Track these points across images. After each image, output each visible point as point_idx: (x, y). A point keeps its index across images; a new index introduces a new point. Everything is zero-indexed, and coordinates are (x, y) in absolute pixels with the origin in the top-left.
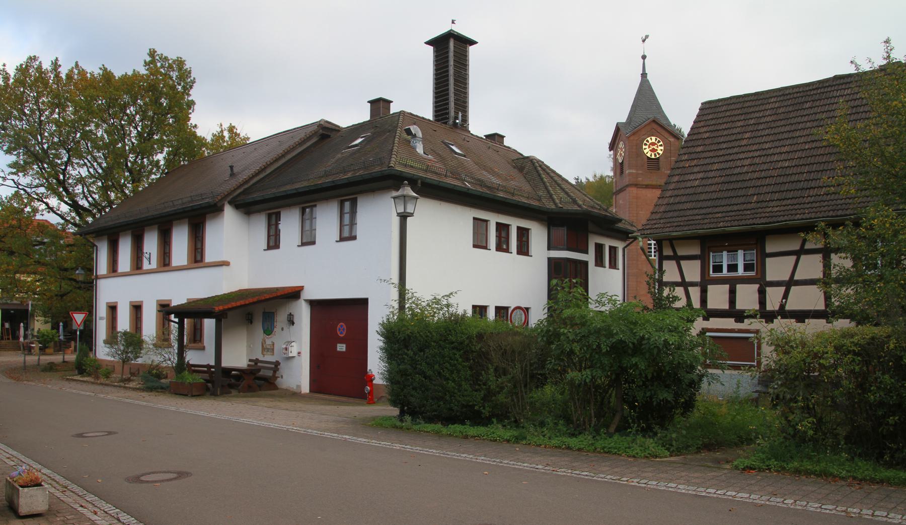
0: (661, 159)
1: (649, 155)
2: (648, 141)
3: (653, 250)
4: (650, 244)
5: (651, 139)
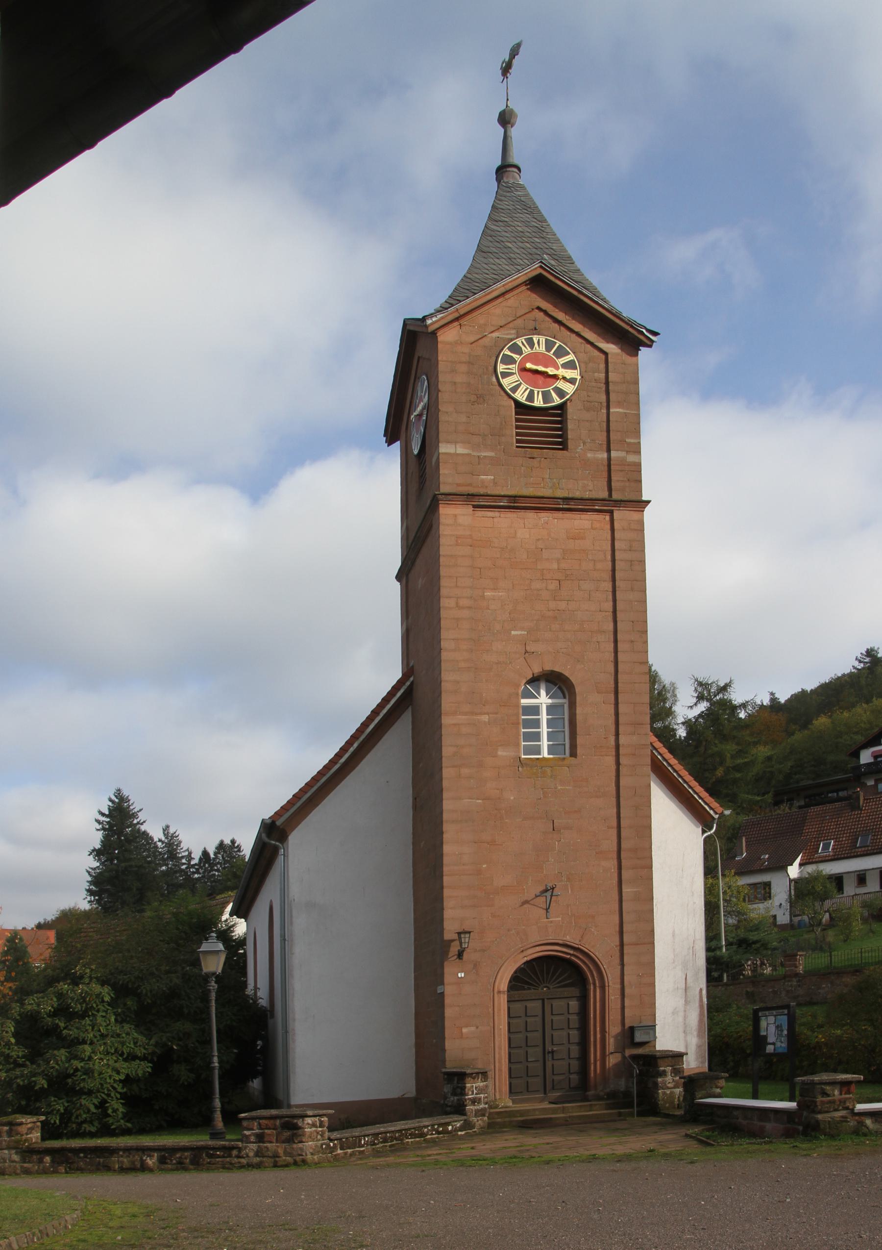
0: (570, 409)
1: (521, 396)
2: (516, 349)
3: (544, 730)
4: (535, 710)
5: (531, 343)
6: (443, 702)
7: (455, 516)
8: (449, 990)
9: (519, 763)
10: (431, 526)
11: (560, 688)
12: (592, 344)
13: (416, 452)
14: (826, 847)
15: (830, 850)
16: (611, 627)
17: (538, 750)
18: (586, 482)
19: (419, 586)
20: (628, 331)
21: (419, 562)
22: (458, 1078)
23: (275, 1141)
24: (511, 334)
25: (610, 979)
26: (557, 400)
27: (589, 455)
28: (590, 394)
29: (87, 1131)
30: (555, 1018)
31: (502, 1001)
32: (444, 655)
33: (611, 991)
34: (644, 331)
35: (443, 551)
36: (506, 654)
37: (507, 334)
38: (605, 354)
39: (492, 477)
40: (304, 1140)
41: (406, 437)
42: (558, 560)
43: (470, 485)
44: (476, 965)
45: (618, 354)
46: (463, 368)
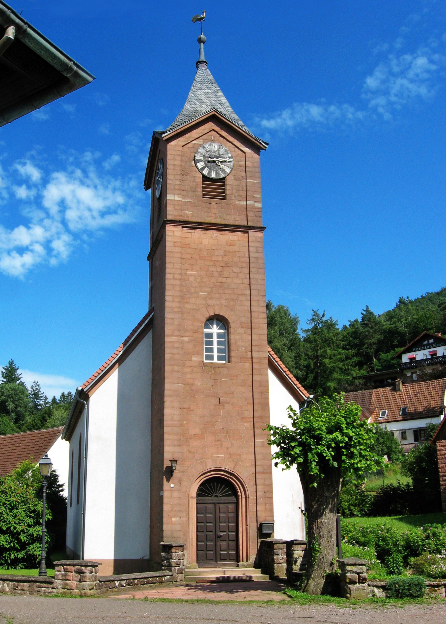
3: (215, 347)
6: (166, 329)
7: (174, 231)
8: (166, 494)
9: (203, 365)
10: (163, 235)
11: (223, 324)
12: (238, 148)
13: (158, 196)
14: (383, 414)
15: (386, 416)
16: (248, 292)
17: (211, 358)
18: (235, 216)
19: (157, 265)
20: (254, 142)
21: (158, 253)
22: (168, 548)
23: (71, 580)
24: (201, 142)
25: (249, 493)
26: (222, 176)
27: (237, 203)
28: (237, 172)
29: (120, 177)
30: (221, 515)
31: (193, 502)
32: (167, 304)
33: (250, 501)
34: (262, 142)
35: (167, 249)
36: (197, 305)
37: (199, 142)
38: (244, 153)
39: (191, 212)
40: (86, 580)
41: (154, 187)
42: (222, 256)
43: (181, 216)
44: (180, 481)
45: (250, 153)
46: (179, 158)
